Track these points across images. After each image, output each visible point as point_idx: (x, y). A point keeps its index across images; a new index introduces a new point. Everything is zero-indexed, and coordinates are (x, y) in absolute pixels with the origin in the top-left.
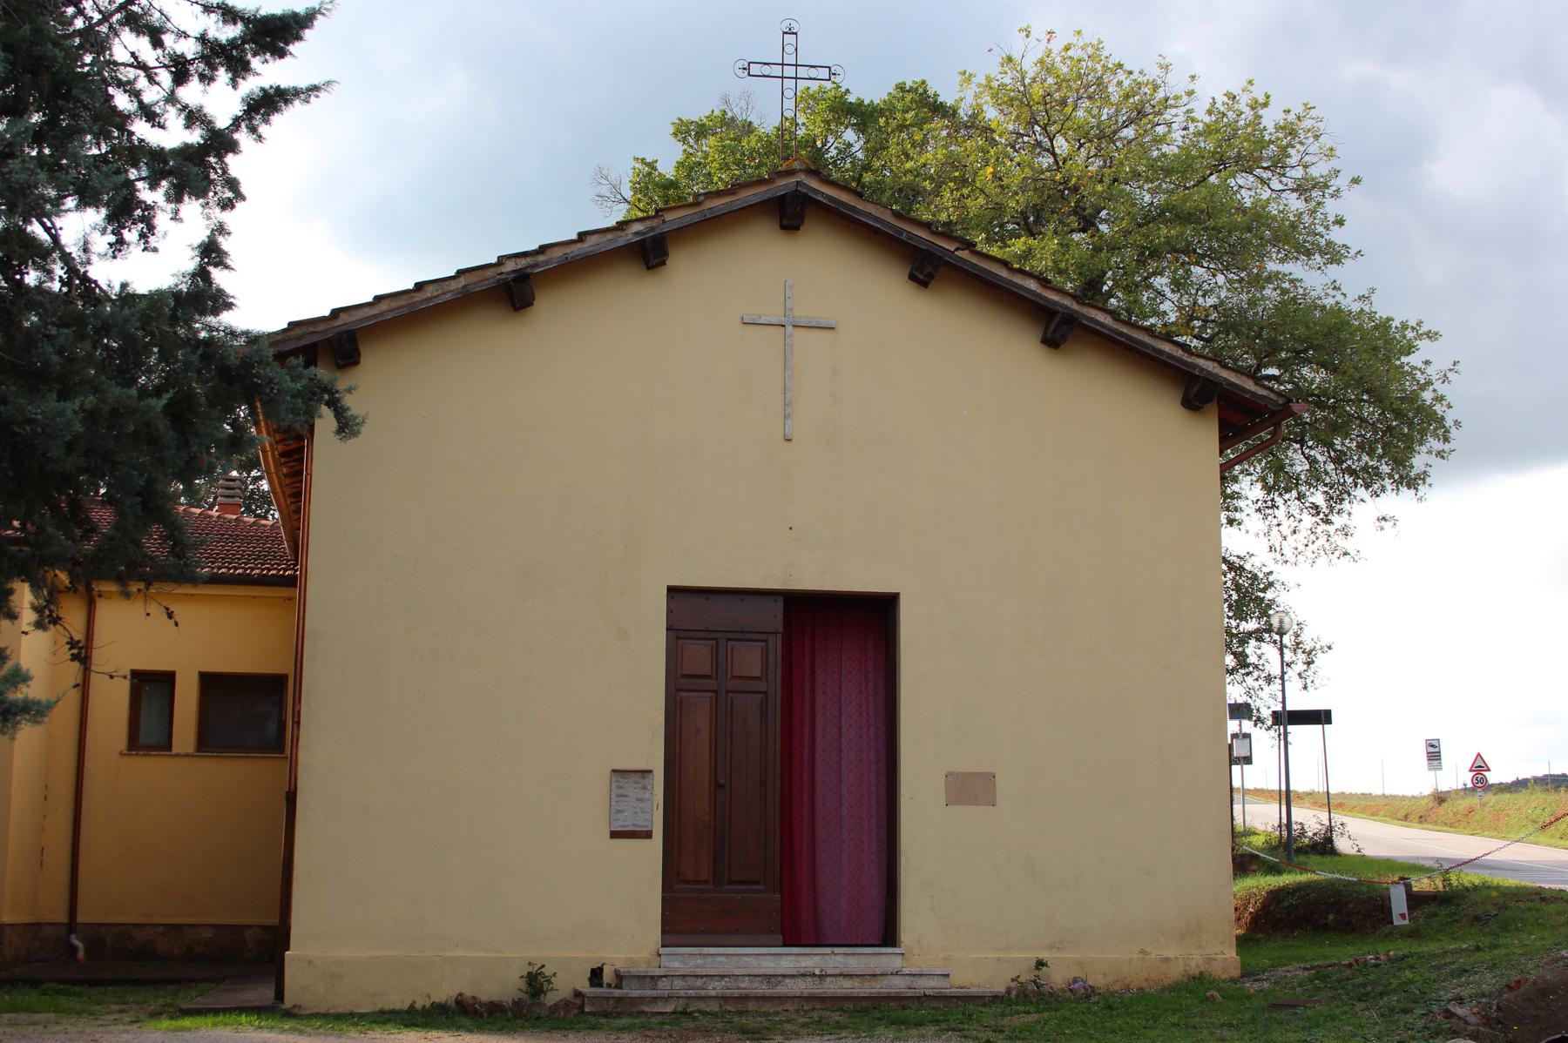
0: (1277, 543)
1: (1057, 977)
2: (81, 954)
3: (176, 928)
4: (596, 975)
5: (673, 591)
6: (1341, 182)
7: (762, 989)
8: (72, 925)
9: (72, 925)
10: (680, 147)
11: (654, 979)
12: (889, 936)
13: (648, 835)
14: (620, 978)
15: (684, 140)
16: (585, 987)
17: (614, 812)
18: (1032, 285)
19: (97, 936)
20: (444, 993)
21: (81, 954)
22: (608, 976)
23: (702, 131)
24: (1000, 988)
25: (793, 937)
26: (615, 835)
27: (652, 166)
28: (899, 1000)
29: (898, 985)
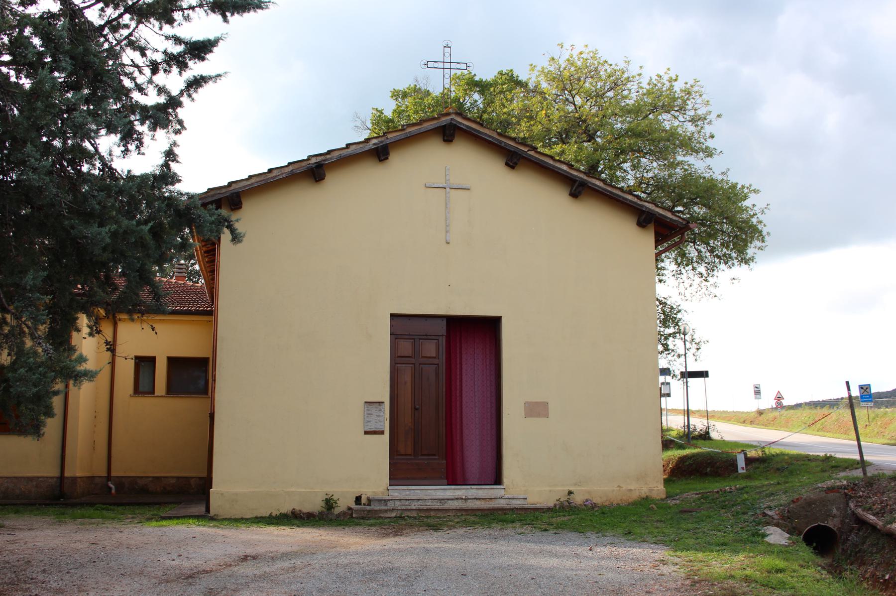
0: (682, 290)
1: (578, 499)
2: (113, 491)
4: (358, 500)
5: (393, 316)
7: (437, 505)
9: (109, 477)
12: (498, 480)
13: (382, 433)
14: (370, 501)
17: (366, 422)
19: (121, 483)
20: (286, 508)
21: (113, 491)
22: (364, 500)
23: (405, 95)
24: (551, 504)
25: (454, 478)
26: (366, 433)
29: (502, 503)
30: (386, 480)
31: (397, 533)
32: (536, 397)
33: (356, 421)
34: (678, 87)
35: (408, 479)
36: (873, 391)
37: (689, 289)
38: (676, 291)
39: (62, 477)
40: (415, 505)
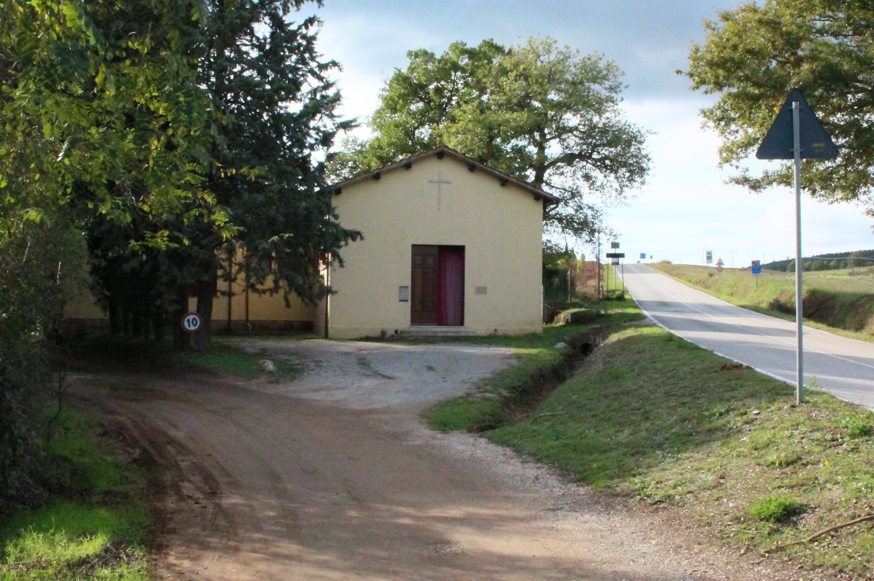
0: (604, 200)
1: (500, 333)
2: (250, 328)
3: (274, 322)
4: (396, 332)
5: (413, 246)
6: (622, 87)
7: (433, 334)
8: (247, 321)
9: (247, 321)
10: (409, 61)
11: (409, 332)
12: (462, 323)
13: (407, 301)
14: (402, 332)
15: (411, 58)
16: (394, 333)
17: (400, 296)
18: (497, 173)
19: (254, 323)
20: (363, 335)
21: (250, 328)
22: (399, 332)
23: (417, 55)
24: (486, 335)
25: (441, 322)
26: (400, 301)
27: (399, 71)
28: (462, 337)
29: (463, 334)
30: (409, 322)
31: (415, 344)
32: (481, 285)
33: (395, 295)
34: (602, 65)
35: (676, 311)
36: (761, 264)
37: (609, 199)
38: (600, 200)
39: (229, 320)
40: (422, 334)
